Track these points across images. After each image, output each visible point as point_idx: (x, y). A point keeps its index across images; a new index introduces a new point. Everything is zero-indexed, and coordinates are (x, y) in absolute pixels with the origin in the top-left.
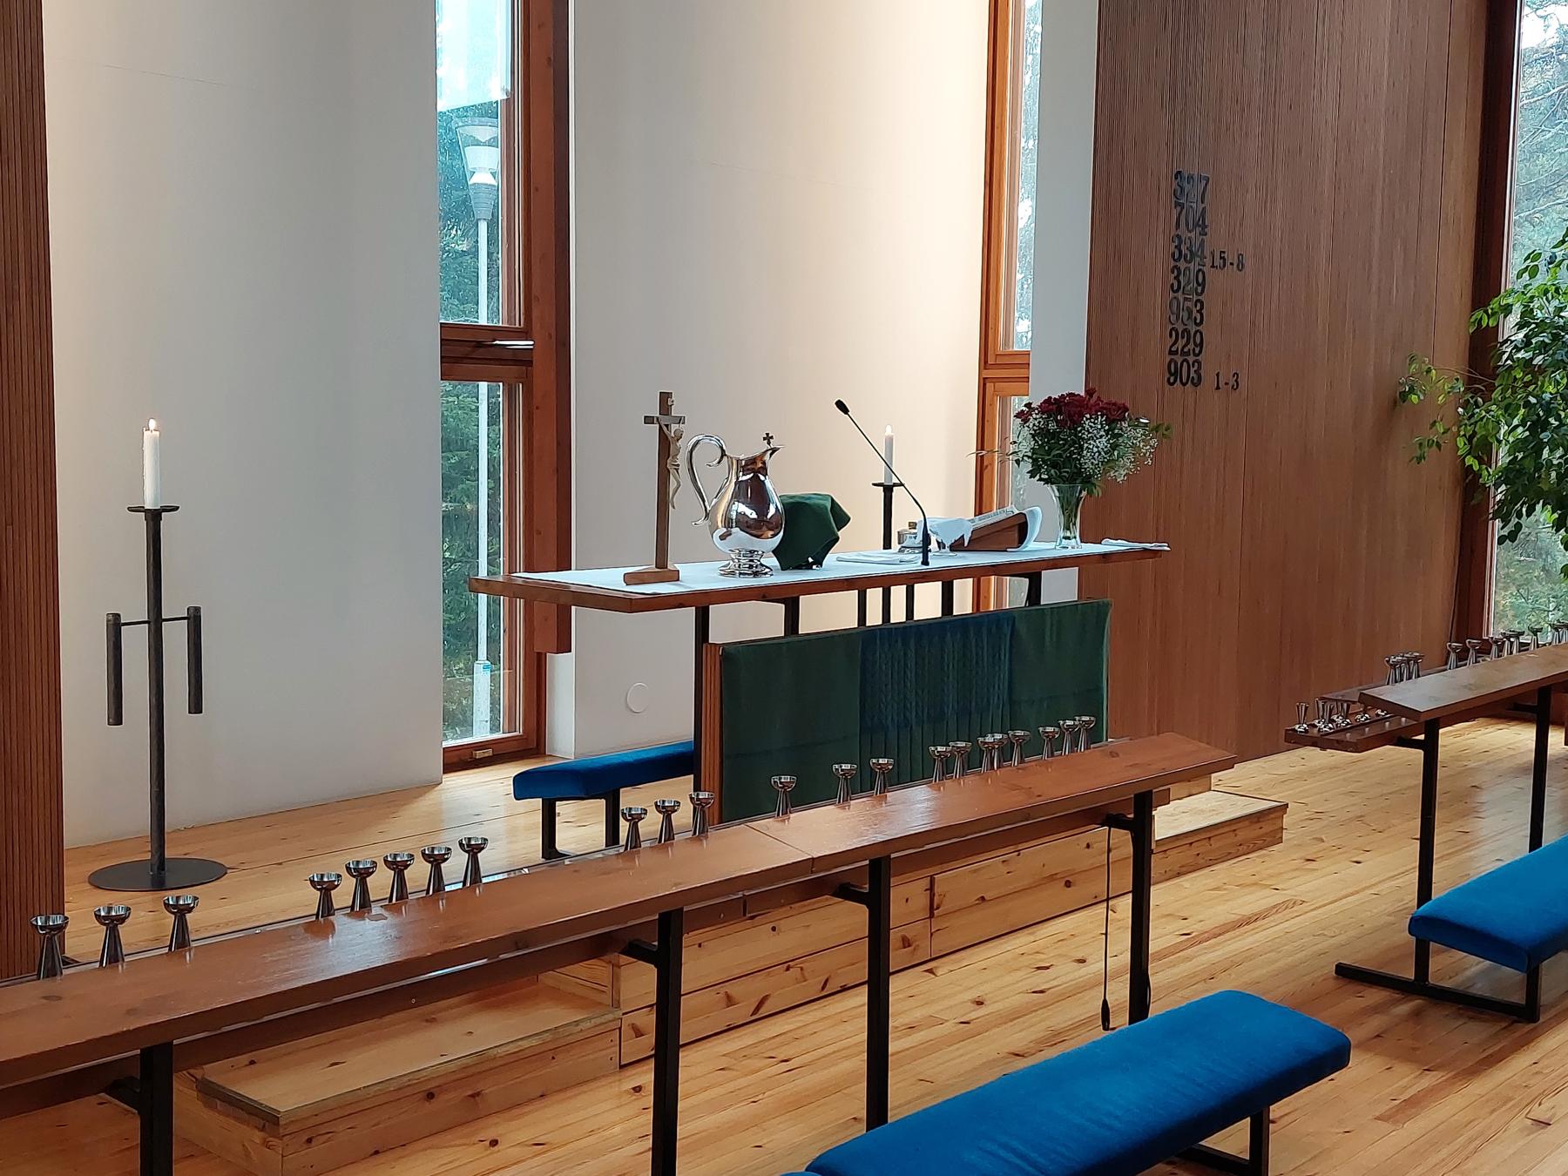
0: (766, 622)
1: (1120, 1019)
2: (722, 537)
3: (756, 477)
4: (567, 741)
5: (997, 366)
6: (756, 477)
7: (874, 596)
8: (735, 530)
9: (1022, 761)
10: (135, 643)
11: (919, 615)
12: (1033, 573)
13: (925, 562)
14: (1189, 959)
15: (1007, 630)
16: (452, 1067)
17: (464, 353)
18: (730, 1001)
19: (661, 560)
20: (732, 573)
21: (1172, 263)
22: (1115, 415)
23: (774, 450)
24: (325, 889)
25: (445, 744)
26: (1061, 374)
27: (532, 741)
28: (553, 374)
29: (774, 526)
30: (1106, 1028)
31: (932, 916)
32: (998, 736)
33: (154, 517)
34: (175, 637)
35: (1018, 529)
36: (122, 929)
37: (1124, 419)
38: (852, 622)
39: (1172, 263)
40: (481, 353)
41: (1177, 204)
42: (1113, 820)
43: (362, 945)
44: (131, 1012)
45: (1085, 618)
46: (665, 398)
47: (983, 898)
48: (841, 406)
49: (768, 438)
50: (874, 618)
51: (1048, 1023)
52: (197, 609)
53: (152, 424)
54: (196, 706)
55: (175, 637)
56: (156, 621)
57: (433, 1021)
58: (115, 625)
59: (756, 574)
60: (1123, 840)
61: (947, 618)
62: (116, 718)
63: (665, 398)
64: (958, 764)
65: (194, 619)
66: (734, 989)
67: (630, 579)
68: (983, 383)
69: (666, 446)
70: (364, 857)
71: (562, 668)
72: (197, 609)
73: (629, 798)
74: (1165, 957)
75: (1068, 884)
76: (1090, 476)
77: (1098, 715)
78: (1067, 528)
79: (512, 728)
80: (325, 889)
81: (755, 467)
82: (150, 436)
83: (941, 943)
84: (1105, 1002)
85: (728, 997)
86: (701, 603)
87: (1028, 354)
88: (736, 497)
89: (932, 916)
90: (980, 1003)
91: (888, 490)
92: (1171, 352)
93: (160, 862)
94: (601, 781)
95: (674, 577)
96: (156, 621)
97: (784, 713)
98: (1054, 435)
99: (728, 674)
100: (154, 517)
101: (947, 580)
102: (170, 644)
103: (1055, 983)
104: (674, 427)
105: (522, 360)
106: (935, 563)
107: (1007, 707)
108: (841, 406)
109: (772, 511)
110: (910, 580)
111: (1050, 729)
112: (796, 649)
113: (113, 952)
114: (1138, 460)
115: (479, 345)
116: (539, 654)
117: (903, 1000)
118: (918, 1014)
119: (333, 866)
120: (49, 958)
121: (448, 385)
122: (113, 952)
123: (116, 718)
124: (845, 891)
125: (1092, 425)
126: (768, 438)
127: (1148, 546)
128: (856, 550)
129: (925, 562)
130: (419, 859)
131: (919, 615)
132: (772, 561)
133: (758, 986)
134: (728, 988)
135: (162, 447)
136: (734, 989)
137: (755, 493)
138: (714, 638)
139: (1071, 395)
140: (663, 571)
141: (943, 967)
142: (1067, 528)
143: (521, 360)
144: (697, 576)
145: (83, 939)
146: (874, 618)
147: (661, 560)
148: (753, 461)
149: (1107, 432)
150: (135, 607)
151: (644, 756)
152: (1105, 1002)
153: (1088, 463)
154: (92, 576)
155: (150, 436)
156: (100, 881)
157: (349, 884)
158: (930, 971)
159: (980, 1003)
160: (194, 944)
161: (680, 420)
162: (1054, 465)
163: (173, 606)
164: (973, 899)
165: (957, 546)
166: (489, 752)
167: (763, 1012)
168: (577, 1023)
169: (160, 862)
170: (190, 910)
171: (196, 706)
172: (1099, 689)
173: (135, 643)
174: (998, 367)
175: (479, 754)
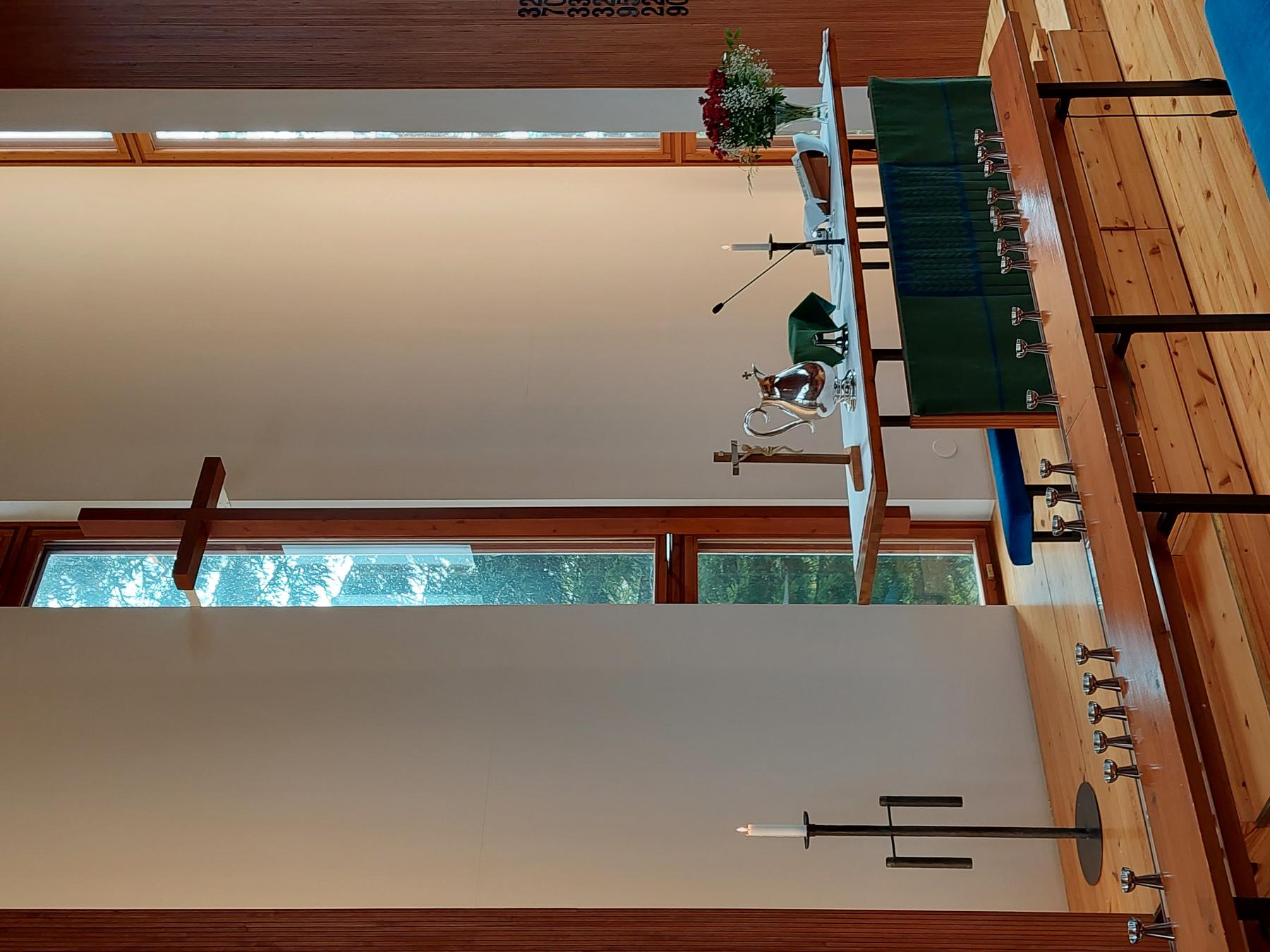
0: (892, 377)
1: (1229, 102)
2: (824, 410)
3: (778, 385)
4: (982, 503)
5: (672, 154)
6: (778, 385)
7: (867, 255)
8: (818, 401)
9: (1013, 193)
10: (909, 846)
11: (879, 203)
12: (851, 149)
13: (842, 242)
14: (1174, 11)
15: (896, 169)
16: (1251, 633)
17: (676, 585)
18: (1201, 403)
19: (844, 460)
20: (853, 402)
21: (591, 15)
22: (719, 82)
23: (756, 371)
24: (1117, 771)
25: (982, 602)
26: (683, 109)
27: (981, 532)
28: (692, 520)
29: (816, 369)
30: (1235, 113)
31: (1133, 229)
32: (992, 214)
33: (813, 830)
34: (903, 816)
35: (813, 159)
36: (1137, 875)
37: (723, 74)
38: (888, 274)
39: (591, 15)
40: (676, 570)
41: (544, 14)
42: (1061, 113)
43: (1144, 674)
44: (1211, 929)
45: (882, 97)
46: (718, 458)
47: (1119, 184)
48: (717, 309)
49: (746, 376)
50: (884, 255)
51: (1228, 141)
52: (882, 799)
53: (742, 830)
54: (957, 802)
55: (903, 816)
56: (891, 830)
57: (1213, 643)
58: (895, 861)
59: (853, 383)
60: (1077, 105)
61: (891, 245)
62: (967, 862)
63: (718, 458)
64: (1014, 249)
65: (889, 801)
66: (1192, 401)
67: (859, 486)
68: (686, 162)
69: (755, 457)
70: (1078, 682)
71: (921, 509)
72: (882, 799)
73: (1033, 477)
74: (1172, 30)
75: (1119, 184)
76: (770, 98)
77: (1128, 917)
78: (811, 115)
79: (970, 548)
80: (1117, 771)
81: (769, 385)
82: (750, 831)
83: (1157, 221)
84: (1213, 115)
85: (1198, 405)
86: (878, 422)
87: (663, 134)
88: (791, 400)
89: (1133, 229)
90: (1209, 194)
91: (776, 247)
92: (662, 14)
93: (1079, 831)
94: (1019, 496)
95: (856, 450)
96: (891, 830)
97: (964, 353)
98: (737, 130)
99: (932, 405)
100: (813, 830)
101: (853, 212)
102: (912, 821)
103: (1193, 130)
104: (740, 450)
105: (679, 542)
106: (841, 232)
107: (960, 167)
108: (717, 309)
109: (803, 372)
110: (856, 246)
111: (986, 169)
112: (916, 350)
113: (1154, 881)
114: (757, 59)
115: (670, 571)
116: (911, 527)
117: (1204, 258)
118: (1217, 247)
119: (1084, 703)
120: (1156, 926)
121: (701, 594)
122: (1154, 881)
123: (967, 862)
124: (1120, 349)
125: (729, 100)
126: (746, 376)
127: (825, 47)
128: (830, 277)
129: (842, 242)
130: (1098, 726)
131: (879, 203)
132: (840, 367)
133: (1190, 379)
134: (1192, 403)
135: (758, 823)
136: (1192, 401)
137: (790, 384)
138: (906, 412)
139: (704, 117)
140: (853, 457)
141: (1177, 219)
142: (811, 115)
143: (681, 547)
144: (854, 429)
145: (1143, 901)
146: (884, 255)
147: (844, 460)
148: (765, 387)
149: (735, 88)
150: (881, 846)
151: (998, 464)
152: (1213, 115)
153: (758, 102)
154: (860, 882)
155: (750, 831)
156: (1093, 874)
157: (1113, 753)
158: (1180, 230)
159: (1209, 194)
160: (1158, 871)
161: (734, 445)
162: (760, 129)
163: (880, 818)
164: (1120, 193)
165: (827, 209)
166: (989, 567)
167: (1212, 374)
168: (1218, 532)
169: (1079, 831)
170: (1132, 873)
171: (957, 802)
172: (943, 86)
173: (909, 846)
174: (673, 152)
175: (990, 574)
